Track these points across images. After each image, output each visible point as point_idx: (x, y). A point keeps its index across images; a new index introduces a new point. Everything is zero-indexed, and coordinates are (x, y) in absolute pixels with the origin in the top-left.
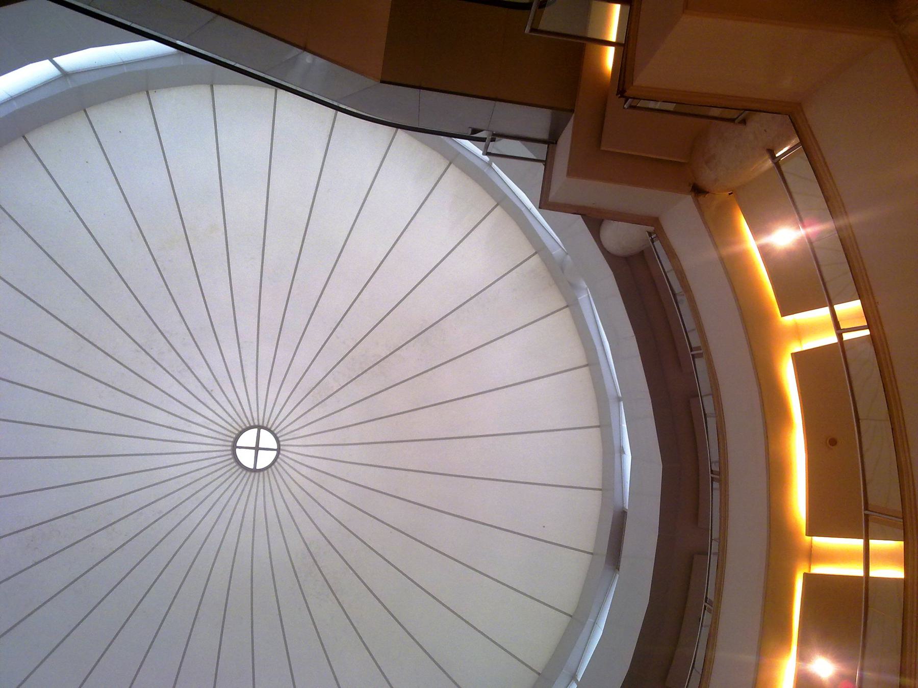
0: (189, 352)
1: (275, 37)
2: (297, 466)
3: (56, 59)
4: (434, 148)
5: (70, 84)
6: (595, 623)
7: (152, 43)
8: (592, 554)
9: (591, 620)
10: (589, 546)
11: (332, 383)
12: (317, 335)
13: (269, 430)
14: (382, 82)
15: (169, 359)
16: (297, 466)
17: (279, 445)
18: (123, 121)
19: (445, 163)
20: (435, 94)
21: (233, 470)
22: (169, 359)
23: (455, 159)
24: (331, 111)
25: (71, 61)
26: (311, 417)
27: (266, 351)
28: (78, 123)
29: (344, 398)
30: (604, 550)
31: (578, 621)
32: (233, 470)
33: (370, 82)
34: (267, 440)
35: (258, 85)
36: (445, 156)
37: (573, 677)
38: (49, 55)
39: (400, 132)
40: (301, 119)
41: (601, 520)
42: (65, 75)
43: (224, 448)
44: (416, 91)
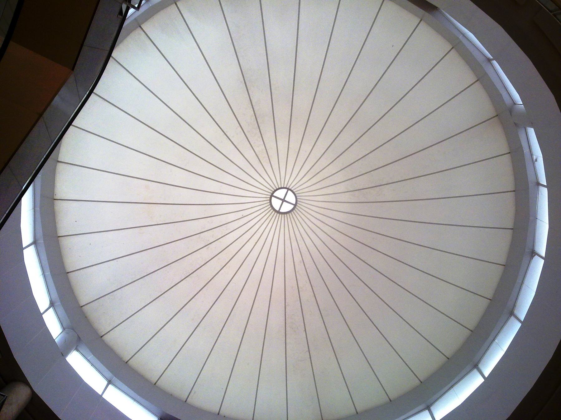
0: (217, 221)
1: (22, 143)
2: (301, 183)
3: (24, 246)
4: (128, 34)
5: (41, 241)
6: (464, 35)
7: (23, 199)
8: (421, 20)
9: (461, 37)
10: (416, 20)
11: (260, 148)
12: (228, 149)
13: (275, 191)
14: (73, 69)
15: (218, 233)
16: (301, 183)
17: (285, 188)
18: (69, 218)
19: (139, 31)
20: (96, 17)
21: (291, 217)
22: (218, 233)
23: (138, 24)
24: (93, 95)
25: (27, 236)
26: (275, 167)
27: (229, 179)
28: (66, 243)
29: (271, 144)
30: (421, 12)
31: (457, 45)
32: (291, 217)
33: (71, 79)
34: (281, 193)
35: (60, 147)
36: (135, 29)
37: (489, 60)
38: (20, 249)
39: (114, 54)
40: (92, 114)
41: (410, 11)
42: (35, 242)
43: (277, 217)
44: (85, 48)
